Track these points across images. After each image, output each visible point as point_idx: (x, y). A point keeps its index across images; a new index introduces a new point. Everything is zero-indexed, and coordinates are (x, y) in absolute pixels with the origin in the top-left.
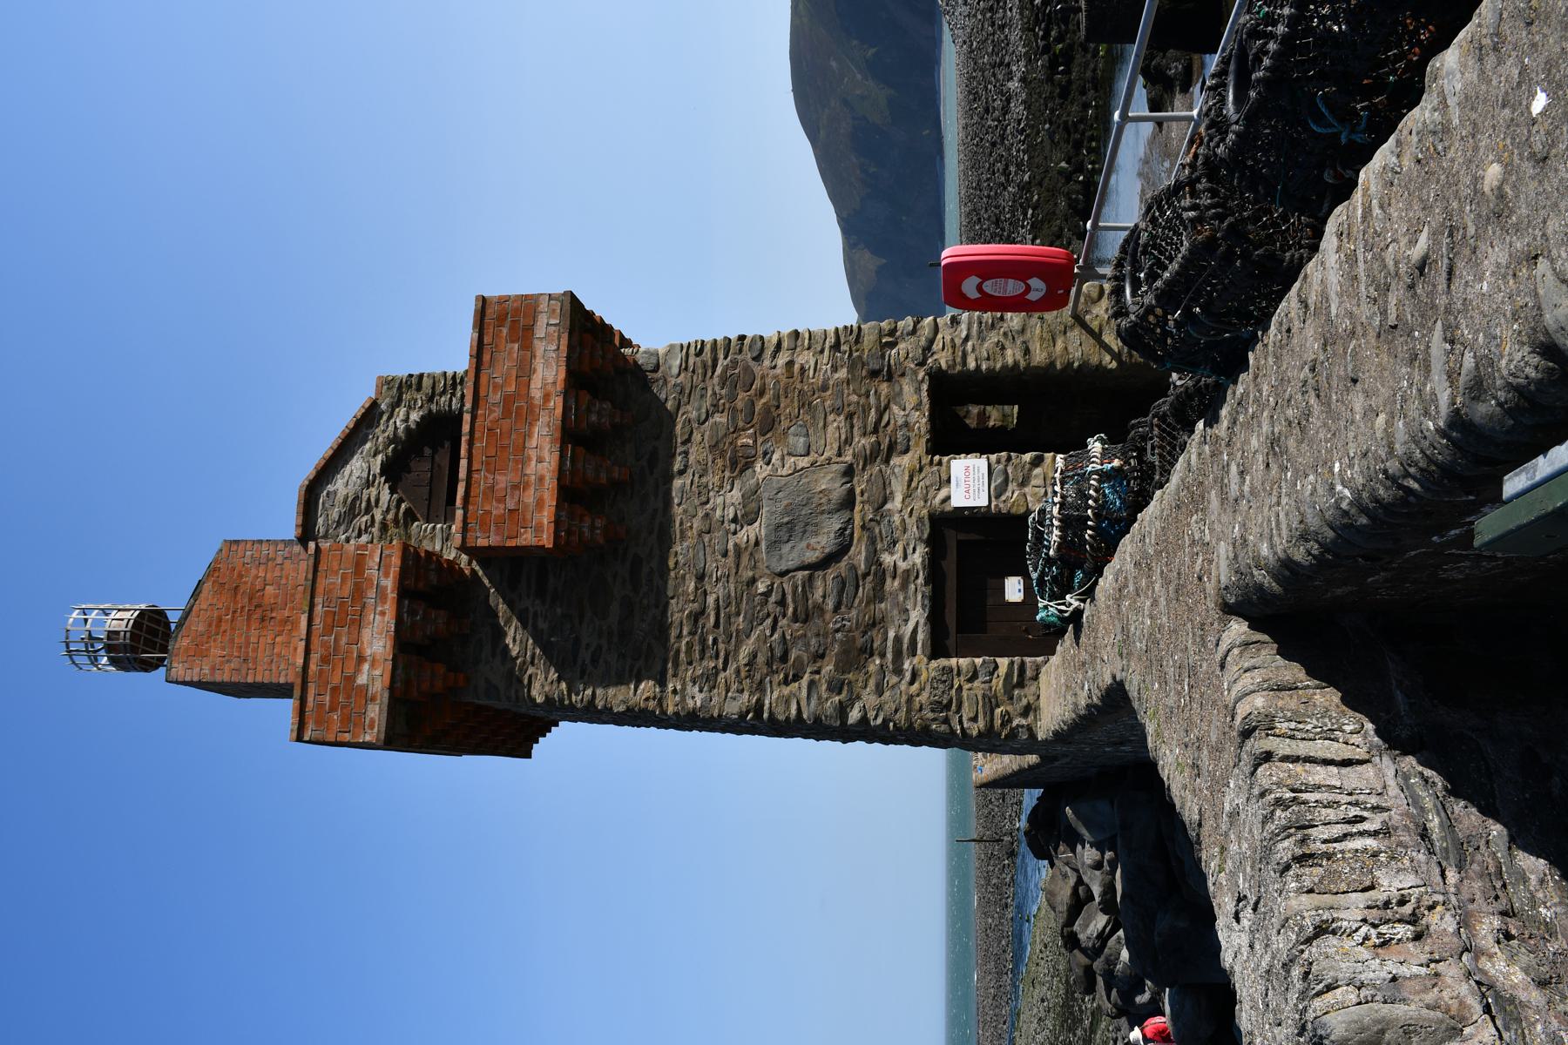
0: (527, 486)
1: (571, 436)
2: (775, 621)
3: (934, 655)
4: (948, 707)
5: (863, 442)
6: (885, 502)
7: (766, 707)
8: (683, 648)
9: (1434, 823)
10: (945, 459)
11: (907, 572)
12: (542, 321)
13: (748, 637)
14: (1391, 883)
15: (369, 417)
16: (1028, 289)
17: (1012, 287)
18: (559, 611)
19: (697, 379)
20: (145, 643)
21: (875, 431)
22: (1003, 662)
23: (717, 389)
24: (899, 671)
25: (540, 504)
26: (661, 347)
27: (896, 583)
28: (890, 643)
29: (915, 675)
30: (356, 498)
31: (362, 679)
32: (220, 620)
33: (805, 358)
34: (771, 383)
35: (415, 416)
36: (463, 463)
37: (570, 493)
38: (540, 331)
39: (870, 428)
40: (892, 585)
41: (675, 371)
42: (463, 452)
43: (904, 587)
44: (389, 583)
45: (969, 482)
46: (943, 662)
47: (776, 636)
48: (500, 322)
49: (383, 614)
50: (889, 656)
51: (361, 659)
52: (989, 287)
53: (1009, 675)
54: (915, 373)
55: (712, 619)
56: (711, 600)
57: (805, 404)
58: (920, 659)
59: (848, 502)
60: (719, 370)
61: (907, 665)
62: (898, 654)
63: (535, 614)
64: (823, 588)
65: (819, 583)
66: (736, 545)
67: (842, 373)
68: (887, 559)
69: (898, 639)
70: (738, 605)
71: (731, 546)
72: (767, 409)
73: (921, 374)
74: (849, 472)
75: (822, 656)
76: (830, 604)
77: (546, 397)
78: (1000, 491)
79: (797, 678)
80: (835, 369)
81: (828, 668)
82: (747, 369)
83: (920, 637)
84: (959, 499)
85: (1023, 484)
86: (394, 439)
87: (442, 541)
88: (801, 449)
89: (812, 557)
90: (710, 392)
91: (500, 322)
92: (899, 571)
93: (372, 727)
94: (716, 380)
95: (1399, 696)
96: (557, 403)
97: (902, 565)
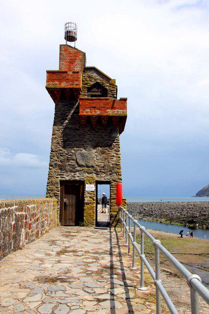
1: (99, 117)
2: (67, 154)
3: (60, 181)
5: (98, 169)
15: (108, 79)
20: (70, 37)
21: (101, 172)
22: (59, 193)
30: (92, 78)
35: (107, 87)
36: (94, 98)
37: (89, 118)
40: (73, 174)
42: (97, 98)
43: (72, 176)
44: (74, 86)
46: (59, 182)
53: (56, 193)
57: (106, 159)
58: (60, 179)
59: (88, 167)
61: (59, 176)
64: (73, 162)
67: (112, 166)
68: (77, 173)
74: (93, 167)
76: (70, 163)
79: (58, 158)
80: (112, 164)
81: (59, 163)
84: (87, 186)
85: (90, 197)
86: (103, 84)
87: (84, 95)
88: (98, 158)
89: (78, 160)
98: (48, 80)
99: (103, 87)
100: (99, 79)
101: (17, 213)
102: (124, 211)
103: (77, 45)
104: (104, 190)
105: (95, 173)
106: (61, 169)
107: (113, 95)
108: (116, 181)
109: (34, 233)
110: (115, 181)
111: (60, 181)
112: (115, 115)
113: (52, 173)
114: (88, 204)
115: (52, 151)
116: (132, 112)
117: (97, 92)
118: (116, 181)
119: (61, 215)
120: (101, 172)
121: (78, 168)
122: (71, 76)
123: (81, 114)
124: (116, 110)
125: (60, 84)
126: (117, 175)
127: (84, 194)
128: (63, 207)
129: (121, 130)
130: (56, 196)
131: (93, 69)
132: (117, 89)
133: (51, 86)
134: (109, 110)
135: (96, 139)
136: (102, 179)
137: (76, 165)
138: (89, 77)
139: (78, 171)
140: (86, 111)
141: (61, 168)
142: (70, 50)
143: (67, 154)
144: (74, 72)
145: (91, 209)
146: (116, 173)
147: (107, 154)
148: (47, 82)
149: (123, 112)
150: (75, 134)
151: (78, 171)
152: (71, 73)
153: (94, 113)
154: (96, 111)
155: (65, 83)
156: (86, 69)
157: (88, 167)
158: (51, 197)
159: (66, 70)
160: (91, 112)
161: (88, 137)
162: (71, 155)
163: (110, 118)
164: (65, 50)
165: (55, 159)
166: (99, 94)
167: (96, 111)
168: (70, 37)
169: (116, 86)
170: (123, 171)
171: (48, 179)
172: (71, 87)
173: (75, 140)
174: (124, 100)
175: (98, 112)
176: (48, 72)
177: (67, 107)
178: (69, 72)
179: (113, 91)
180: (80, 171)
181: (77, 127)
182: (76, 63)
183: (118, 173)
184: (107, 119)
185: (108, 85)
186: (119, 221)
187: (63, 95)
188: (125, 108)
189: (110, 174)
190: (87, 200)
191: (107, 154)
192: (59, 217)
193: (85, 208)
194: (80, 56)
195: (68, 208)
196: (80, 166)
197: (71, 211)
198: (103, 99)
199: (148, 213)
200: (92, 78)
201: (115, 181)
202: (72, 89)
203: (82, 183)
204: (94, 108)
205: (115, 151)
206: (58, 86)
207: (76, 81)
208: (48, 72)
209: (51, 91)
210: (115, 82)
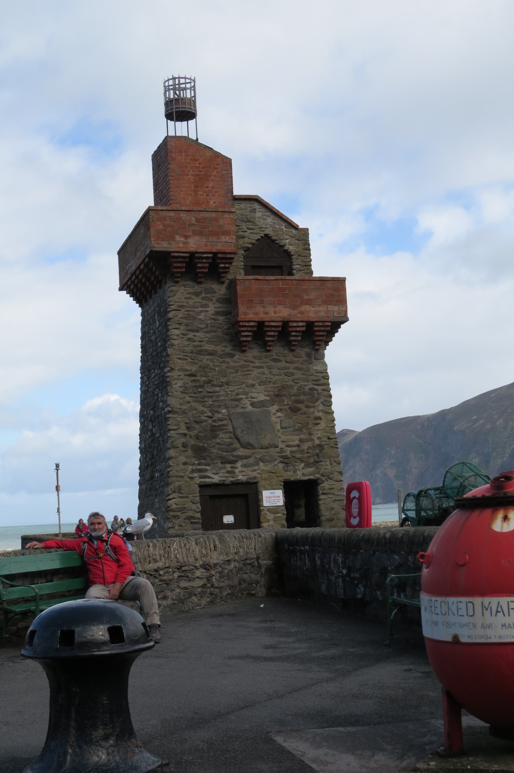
0: (264, 307)
4: (180, 492)
6: (263, 462)
7: (174, 416)
8: (196, 378)
9: (248, 562)
10: (282, 487)
11: (234, 473)
12: (336, 308)
13: (203, 406)
14: (241, 550)
16: (355, 517)
17: (355, 511)
18: (209, 322)
19: (313, 378)
23: (308, 387)
24: (193, 471)
25: (257, 313)
26: (327, 359)
27: (229, 469)
28: (204, 467)
29: (192, 478)
31: (178, 238)
32: (196, 160)
33: (323, 424)
34: (311, 410)
35: (291, 248)
36: (182, 255)
38: (331, 308)
39: (293, 454)
40: (228, 466)
41: (315, 368)
43: (228, 472)
45: (273, 498)
47: (204, 418)
48: (335, 288)
49: (206, 245)
50: (199, 467)
51: (186, 237)
52: (355, 501)
54: (318, 473)
55: (210, 390)
56: (217, 389)
58: (198, 481)
60: (316, 387)
61: (196, 475)
62: (200, 471)
63: (207, 311)
65: (228, 435)
66: (242, 399)
68: (239, 464)
69: (206, 470)
70: (216, 401)
71: (241, 396)
72: (299, 409)
73: (318, 476)
75: (197, 438)
77: (302, 313)
78: (269, 510)
80: (319, 438)
82: (317, 399)
83: (207, 480)
87: (237, 271)
88: (284, 425)
89: (239, 432)
90: (306, 383)
91: (335, 288)
92: (234, 470)
93: (157, 244)
94: (312, 386)
95: (265, 562)
96: (299, 317)
97: (237, 471)
99: (277, 251)
100: (269, 226)
103: (209, 129)
121: (242, 452)
135: (274, 378)
139: (241, 458)
150: (224, 365)
151: (241, 458)
161: (255, 373)
168: (180, 109)
173: (227, 384)
177: (198, 299)
180: (247, 457)
184: (304, 329)
191: (305, 414)
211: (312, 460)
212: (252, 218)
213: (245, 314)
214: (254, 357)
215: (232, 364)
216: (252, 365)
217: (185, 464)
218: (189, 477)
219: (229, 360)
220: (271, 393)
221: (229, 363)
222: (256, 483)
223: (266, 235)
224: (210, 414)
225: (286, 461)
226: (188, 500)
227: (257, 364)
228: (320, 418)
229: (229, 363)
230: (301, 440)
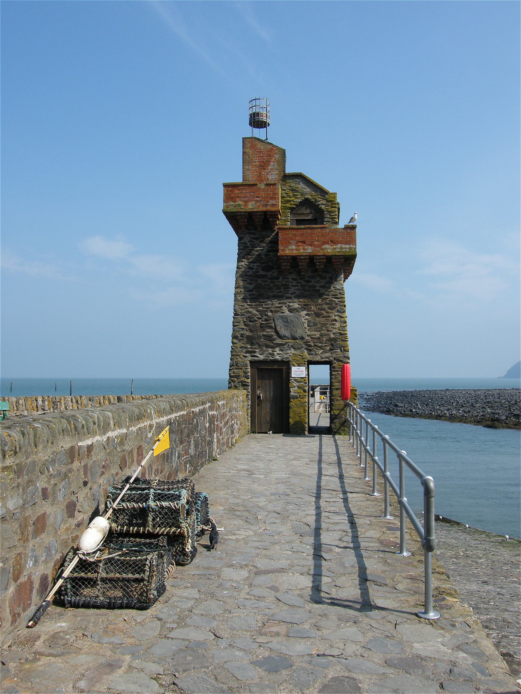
1: (311, 258)
2: (260, 318)
3: (251, 362)
15: (323, 192)
19: (332, 293)
20: (256, 121)
21: (315, 346)
22: (249, 381)
29: (245, 357)
30: (298, 192)
35: (323, 207)
36: (303, 227)
37: (294, 258)
40: (270, 350)
44: (269, 208)
46: (249, 364)
53: (245, 382)
58: (250, 358)
59: (294, 338)
60: (334, 299)
61: (248, 355)
68: (277, 349)
72: (322, 314)
76: (265, 333)
79: (245, 325)
84: (294, 369)
85: (299, 387)
86: (316, 201)
87: (286, 221)
89: (278, 328)
97: (275, 353)
98: (228, 198)
99: (316, 208)
101: (211, 413)
102: (354, 408)
103: (273, 135)
104: (321, 374)
105: (306, 349)
106: (252, 344)
107: (332, 218)
108: (341, 361)
109: (225, 440)
110: (339, 361)
111: (251, 362)
112: (338, 254)
113: (237, 350)
114: (297, 398)
115: (235, 314)
116: (363, 247)
117: (307, 214)
118: (341, 361)
119: (253, 416)
120: (315, 346)
121: (279, 341)
122: (263, 190)
123: (280, 253)
124: (339, 246)
125: (246, 205)
126: (341, 351)
127: (289, 382)
128: (256, 402)
129: (348, 272)
130: (244, 385)
131: (299, 176)
132: (339, 209)
133: (231, 209)
134: (327, 246)
136: (318, 358)
137: (275, 337)
138: (293, 190)
140: (290, 247)
141: (250, 340)
142: (260, 146)
143: (260, 318)
144: (267, 185)
145: (301, 406)
146: (340, 348)
147: (326, 317)
148: (224, 202)
149: (350, 248)
152: (263, 186)
153: (302, 251)
154: (306, 247)
155: (254, 203)
156: (286, 177)
157: (294, 338)
158: (236, 387)
159: (255, 183)
160: (297, 250)
161: (292, 290)
162: (266, 320)
163: (329, 259)
164: (253, 147)
165: (241, 327)
166: (310, 217)
167: (306, 247)
168: (256, 121)
169: (338, 203)
170: (351, 344)
171: (231, 359)
172: (264, 209)
174: (351, 228)
175: (309, 250)
176: (226, 186)
178: (259, 185)
179: (332, 212)
180: (283, 345)
181: (275, 275)
182: (270, 167)
183: (344, 347)
185: (324, 202)
186: (345, 424)
187: (251, 225)
188: (352, 240)
189: (331, 350)
190: (293, 391)
191: (326, 317)
192: (250, 418)
193: (291, 404)
194: (277, 156)
195: (263, 405)
196: (280, 337)
197: (266, 409)
198: (317, 228)
199: (396, 403)
200: (298, 192)
201: (339, 361)
202: (265, 213)
203: (286, 365)
204: (304, 242)
205: (338, 311)
206: (243, 209)
207: (272, 198)
208: (226, 186)
209: (232, 217)
210: (335, 197)
211: (328, 348)
212: (296, 188)
213: (283, 250)
214: (293, 279)
215: (277, 283)
216: (290, 284)
217: (241, 347)
218: (244, 356)
219: (275, 281)
220: (303, 303)
221: (275, 282)
222: (289, 361)
223: (306, 199)
224: (260, 316)
225: (310, 348)
226: (242, 370)
227: (294, 284)
228: (336, 320)
229: (275, 282)
230: (321, 335)
